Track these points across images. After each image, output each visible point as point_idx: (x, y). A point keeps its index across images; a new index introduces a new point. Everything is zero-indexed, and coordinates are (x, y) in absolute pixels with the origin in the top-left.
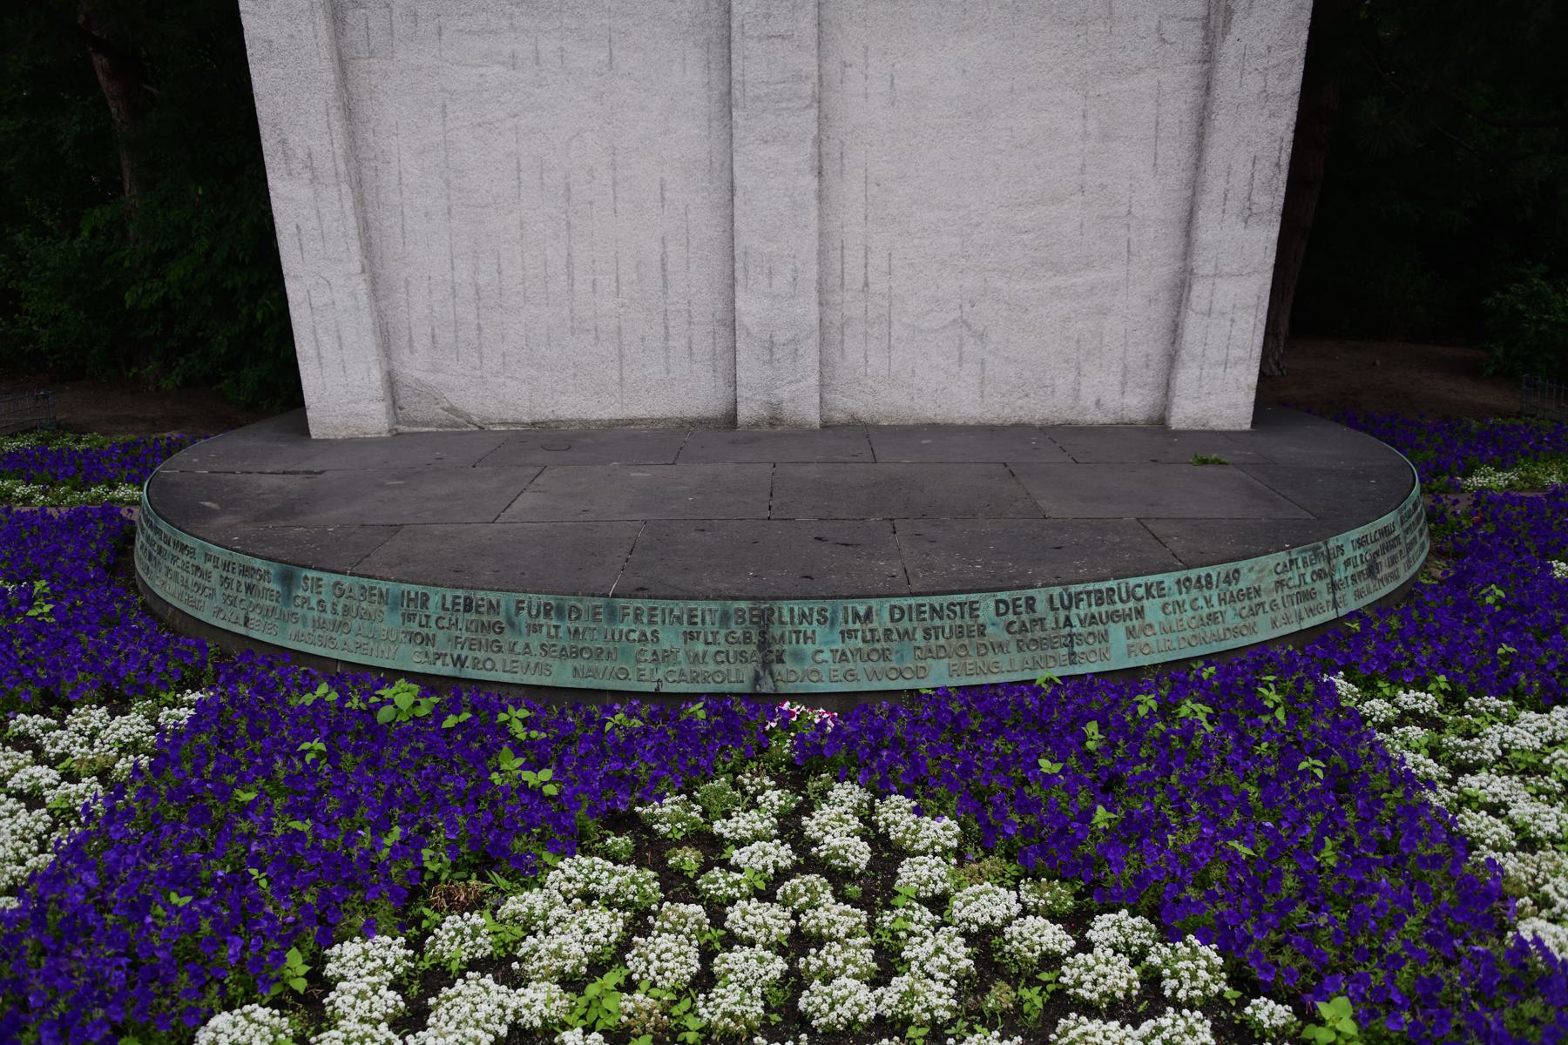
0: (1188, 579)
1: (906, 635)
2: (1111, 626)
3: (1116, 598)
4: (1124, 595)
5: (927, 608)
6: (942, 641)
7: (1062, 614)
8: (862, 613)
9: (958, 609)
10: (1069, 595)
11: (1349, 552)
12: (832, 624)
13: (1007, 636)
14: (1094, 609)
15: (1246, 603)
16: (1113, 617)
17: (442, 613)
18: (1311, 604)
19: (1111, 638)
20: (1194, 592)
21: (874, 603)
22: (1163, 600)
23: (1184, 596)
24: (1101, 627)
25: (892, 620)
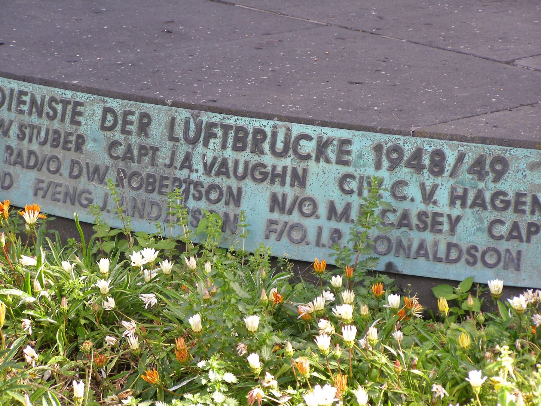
0: (397, 149)
2: (248, 185)
3: (266, 146)
4: (280, 146)
5: (27, 99)
7: (183, 149)
9: (59, 107)
10: (199, 125)
13: (108, 161)
14: (229, 153)
16: (259, 174)
20: (403, 173)
22: (344, 170)
23: (384, 173)
24: (233, 183)
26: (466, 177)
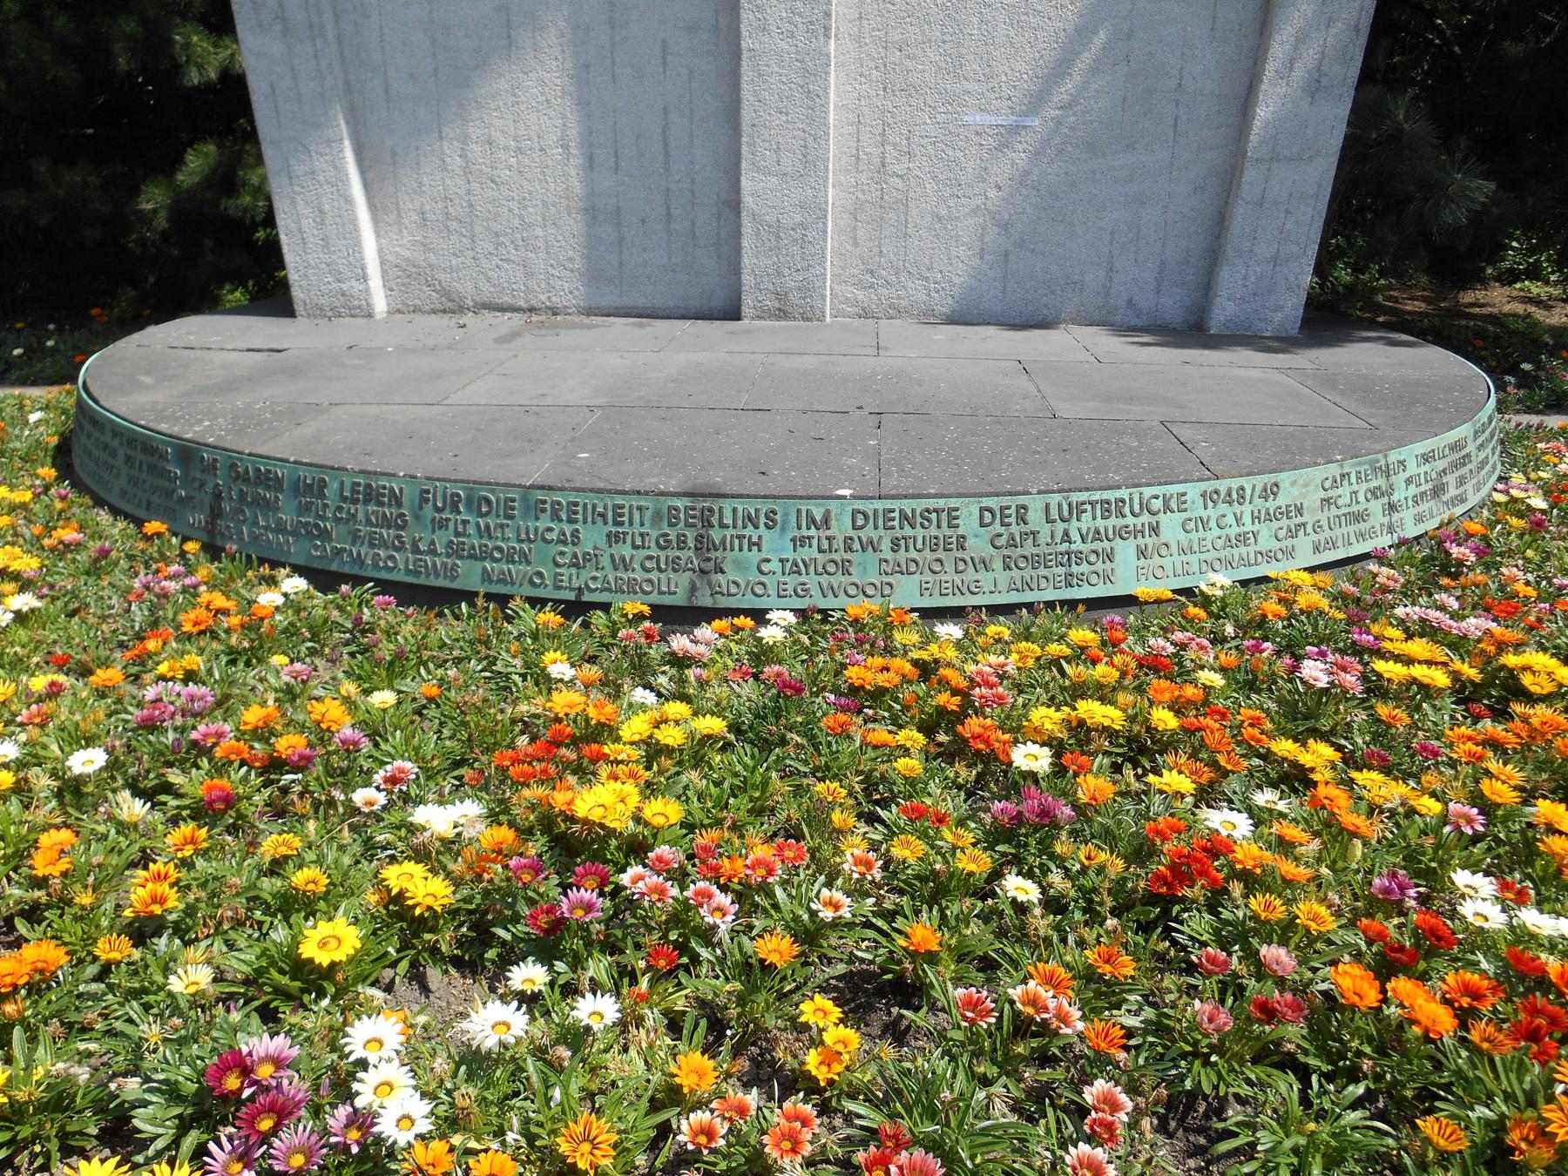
3: (1127, 510)
6: (913, 554)
7: (1060, 527)
8: (818, 518)
11: (1412, 468)
12: (783, 529)
14: (1100, 523)
15: (1284, 522)
16: (1122, 533)
18: (1362, 526)
19: (1117, 558)
24: (1106, 544)
26: (1258, 501)
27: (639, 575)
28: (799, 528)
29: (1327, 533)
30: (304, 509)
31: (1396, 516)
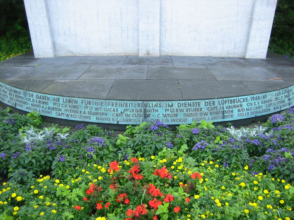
1: (182, 110)
2: (234, 109)
3: (235, 102)
6: (191, 112)
7: (222, 106)
8: (170, 105)
12: (163, 108)
13: (208, 111)
14: (230, 104)
15: (268, 103)
16: (235, 107)
17: (63, 103)
18: (284, 104)
20: (255, 101)
21: (173, 102)
24: (231, 109)
25: (178, 106)
27: (131, 118)
28: (166, 107)
29: (277, 105)
30: (55, 104)
31: (290, 101)
